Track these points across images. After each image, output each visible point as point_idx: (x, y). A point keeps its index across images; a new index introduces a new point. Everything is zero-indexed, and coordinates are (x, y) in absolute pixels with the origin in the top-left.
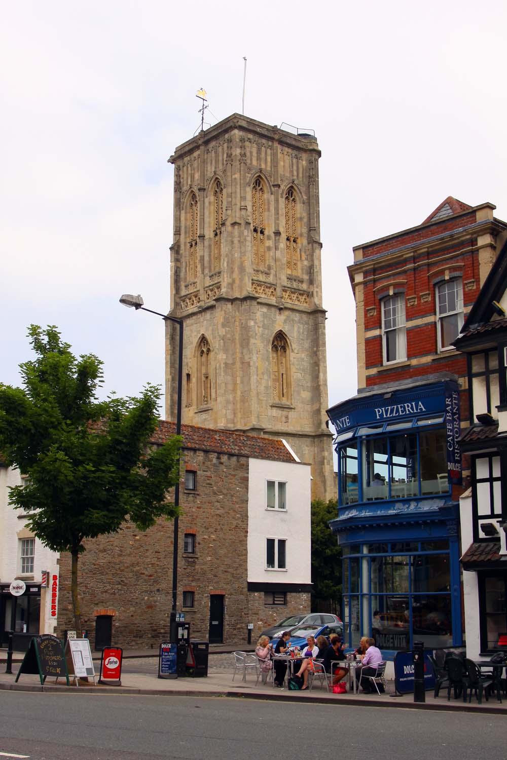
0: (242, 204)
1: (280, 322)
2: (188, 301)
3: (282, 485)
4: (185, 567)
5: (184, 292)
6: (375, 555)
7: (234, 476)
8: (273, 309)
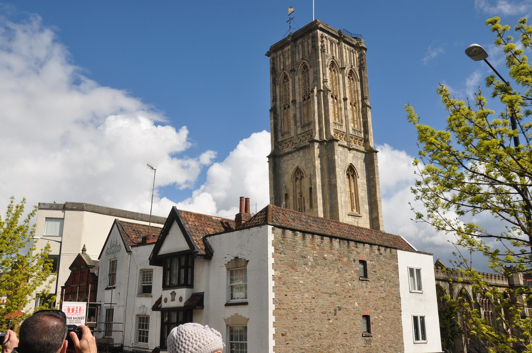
0: (324, 78)
2: (284, 145)
3: (418, 271)
4: (365, 345)
5: (280, 139)
7: (389, 264)
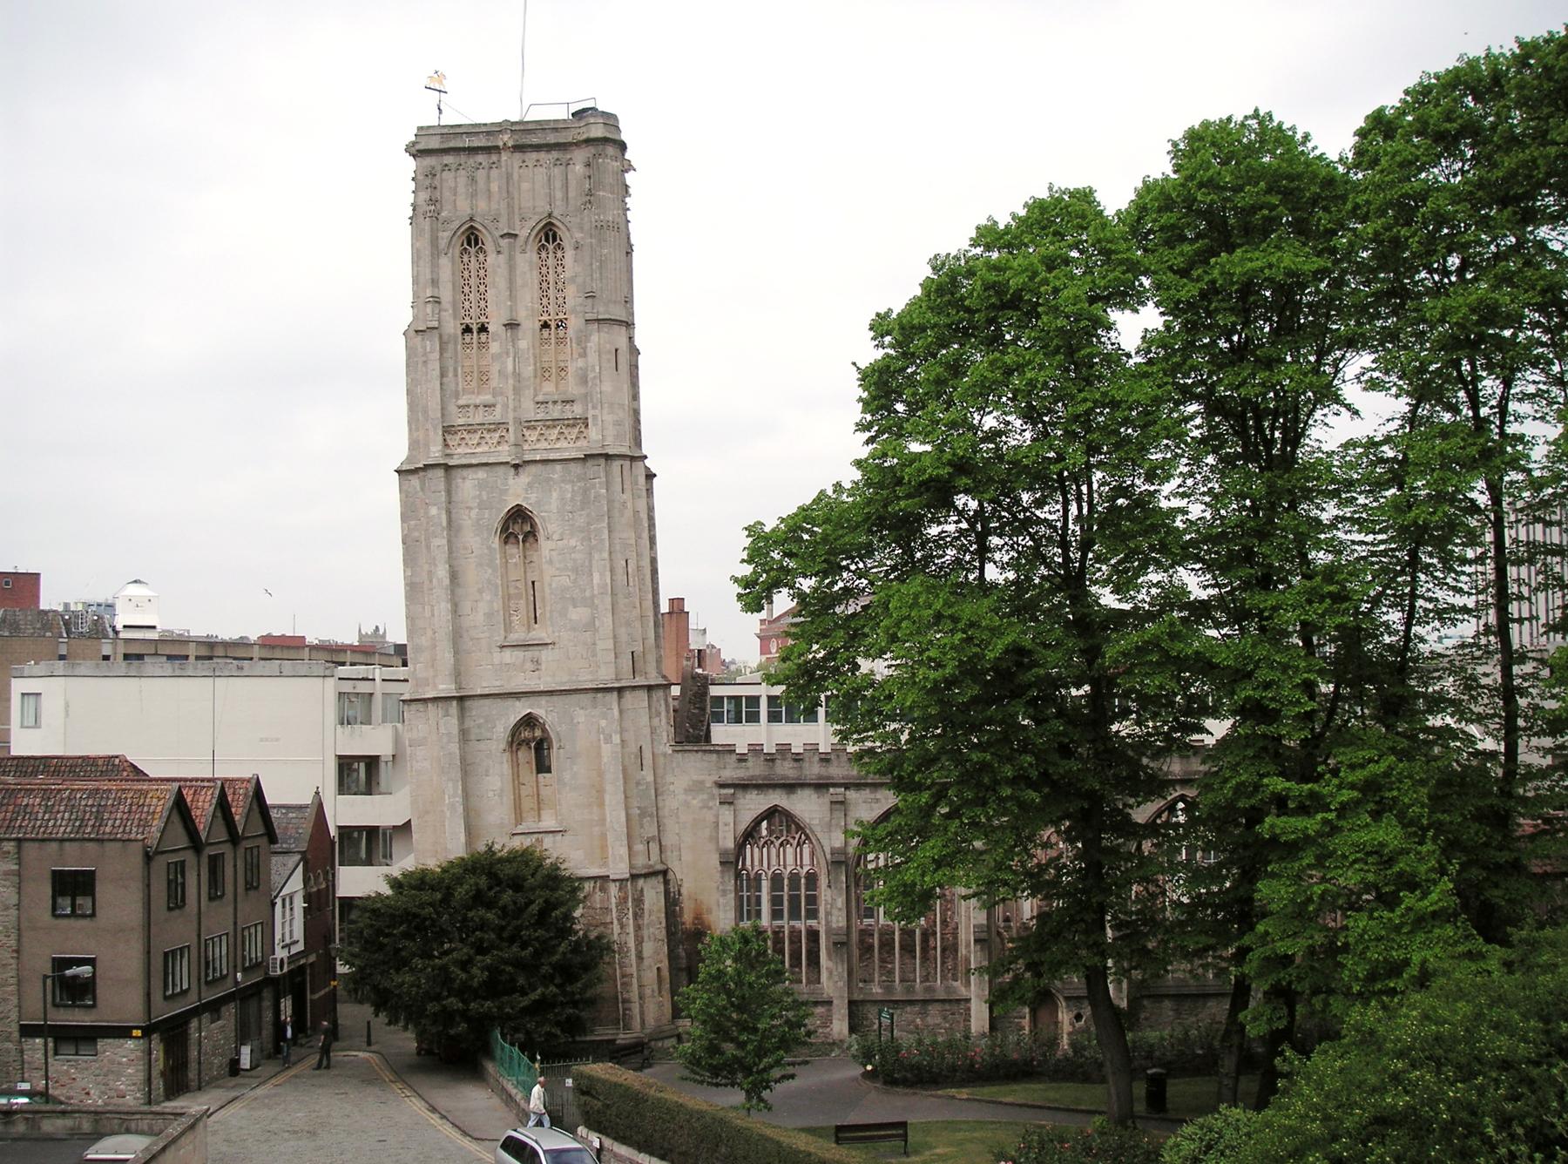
1: (517, 490)
6: (786, 903)
8: (501, 469)
